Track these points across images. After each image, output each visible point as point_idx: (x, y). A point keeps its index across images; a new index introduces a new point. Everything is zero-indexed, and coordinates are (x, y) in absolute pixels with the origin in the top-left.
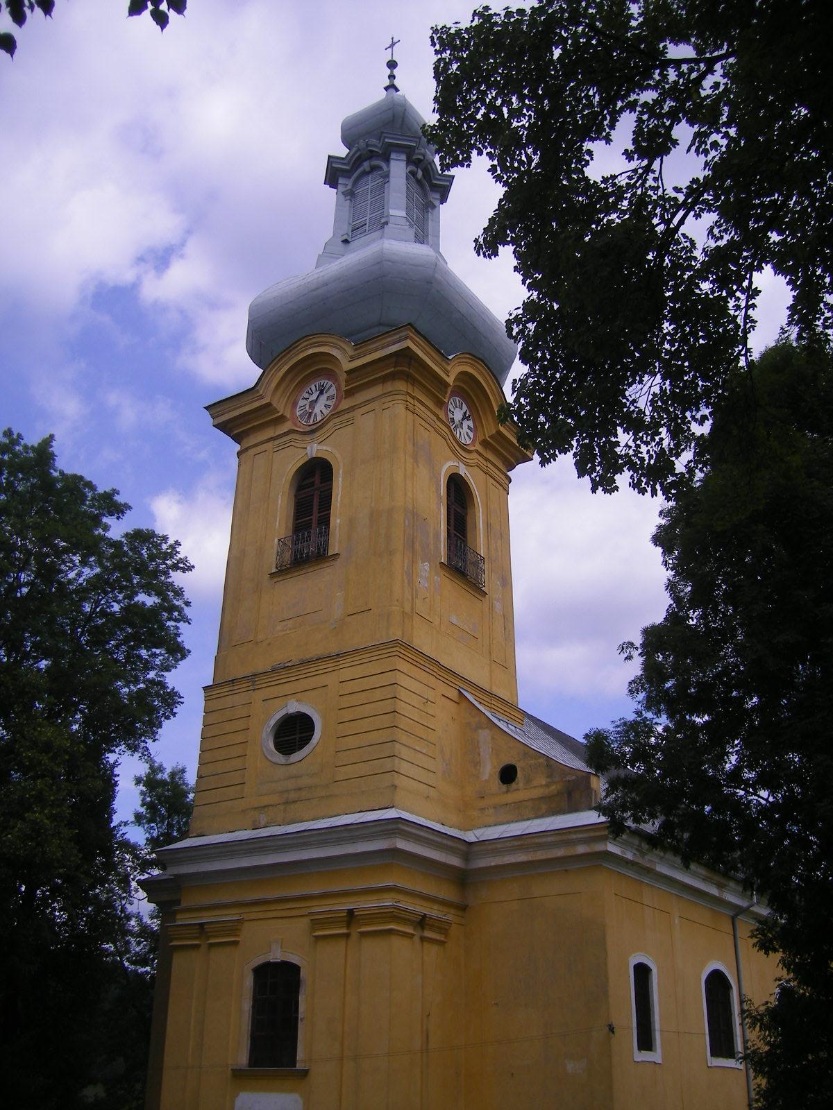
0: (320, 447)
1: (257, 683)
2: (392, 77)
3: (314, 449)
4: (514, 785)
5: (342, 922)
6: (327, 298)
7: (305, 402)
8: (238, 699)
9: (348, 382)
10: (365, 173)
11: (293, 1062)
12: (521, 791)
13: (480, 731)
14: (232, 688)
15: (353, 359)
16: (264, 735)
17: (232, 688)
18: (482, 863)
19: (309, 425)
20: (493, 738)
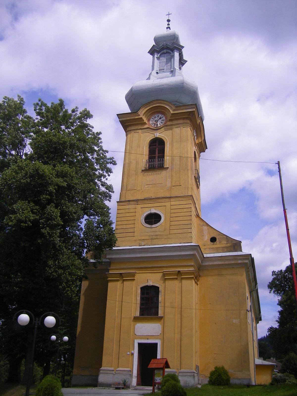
0: (159, 135)
1: (139, 202)
2: (168, 24)
3: (158, 135)
4: (215, 243)
5: (175, 274)
6: (163, 90)
7: (153, 120)
8: (130, 206)
9: (171, 117)
10: (164, 53)
11: (157, 313)
12: (217, 245)
13: (204, 227)
14: (129, 203)
15: (174, 110)
16: (142, 218)
17: (129, 203)
18: (207, 264)
19: (155, 127)
20: (208, 229)
